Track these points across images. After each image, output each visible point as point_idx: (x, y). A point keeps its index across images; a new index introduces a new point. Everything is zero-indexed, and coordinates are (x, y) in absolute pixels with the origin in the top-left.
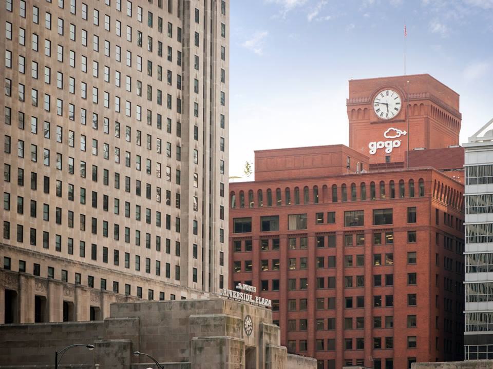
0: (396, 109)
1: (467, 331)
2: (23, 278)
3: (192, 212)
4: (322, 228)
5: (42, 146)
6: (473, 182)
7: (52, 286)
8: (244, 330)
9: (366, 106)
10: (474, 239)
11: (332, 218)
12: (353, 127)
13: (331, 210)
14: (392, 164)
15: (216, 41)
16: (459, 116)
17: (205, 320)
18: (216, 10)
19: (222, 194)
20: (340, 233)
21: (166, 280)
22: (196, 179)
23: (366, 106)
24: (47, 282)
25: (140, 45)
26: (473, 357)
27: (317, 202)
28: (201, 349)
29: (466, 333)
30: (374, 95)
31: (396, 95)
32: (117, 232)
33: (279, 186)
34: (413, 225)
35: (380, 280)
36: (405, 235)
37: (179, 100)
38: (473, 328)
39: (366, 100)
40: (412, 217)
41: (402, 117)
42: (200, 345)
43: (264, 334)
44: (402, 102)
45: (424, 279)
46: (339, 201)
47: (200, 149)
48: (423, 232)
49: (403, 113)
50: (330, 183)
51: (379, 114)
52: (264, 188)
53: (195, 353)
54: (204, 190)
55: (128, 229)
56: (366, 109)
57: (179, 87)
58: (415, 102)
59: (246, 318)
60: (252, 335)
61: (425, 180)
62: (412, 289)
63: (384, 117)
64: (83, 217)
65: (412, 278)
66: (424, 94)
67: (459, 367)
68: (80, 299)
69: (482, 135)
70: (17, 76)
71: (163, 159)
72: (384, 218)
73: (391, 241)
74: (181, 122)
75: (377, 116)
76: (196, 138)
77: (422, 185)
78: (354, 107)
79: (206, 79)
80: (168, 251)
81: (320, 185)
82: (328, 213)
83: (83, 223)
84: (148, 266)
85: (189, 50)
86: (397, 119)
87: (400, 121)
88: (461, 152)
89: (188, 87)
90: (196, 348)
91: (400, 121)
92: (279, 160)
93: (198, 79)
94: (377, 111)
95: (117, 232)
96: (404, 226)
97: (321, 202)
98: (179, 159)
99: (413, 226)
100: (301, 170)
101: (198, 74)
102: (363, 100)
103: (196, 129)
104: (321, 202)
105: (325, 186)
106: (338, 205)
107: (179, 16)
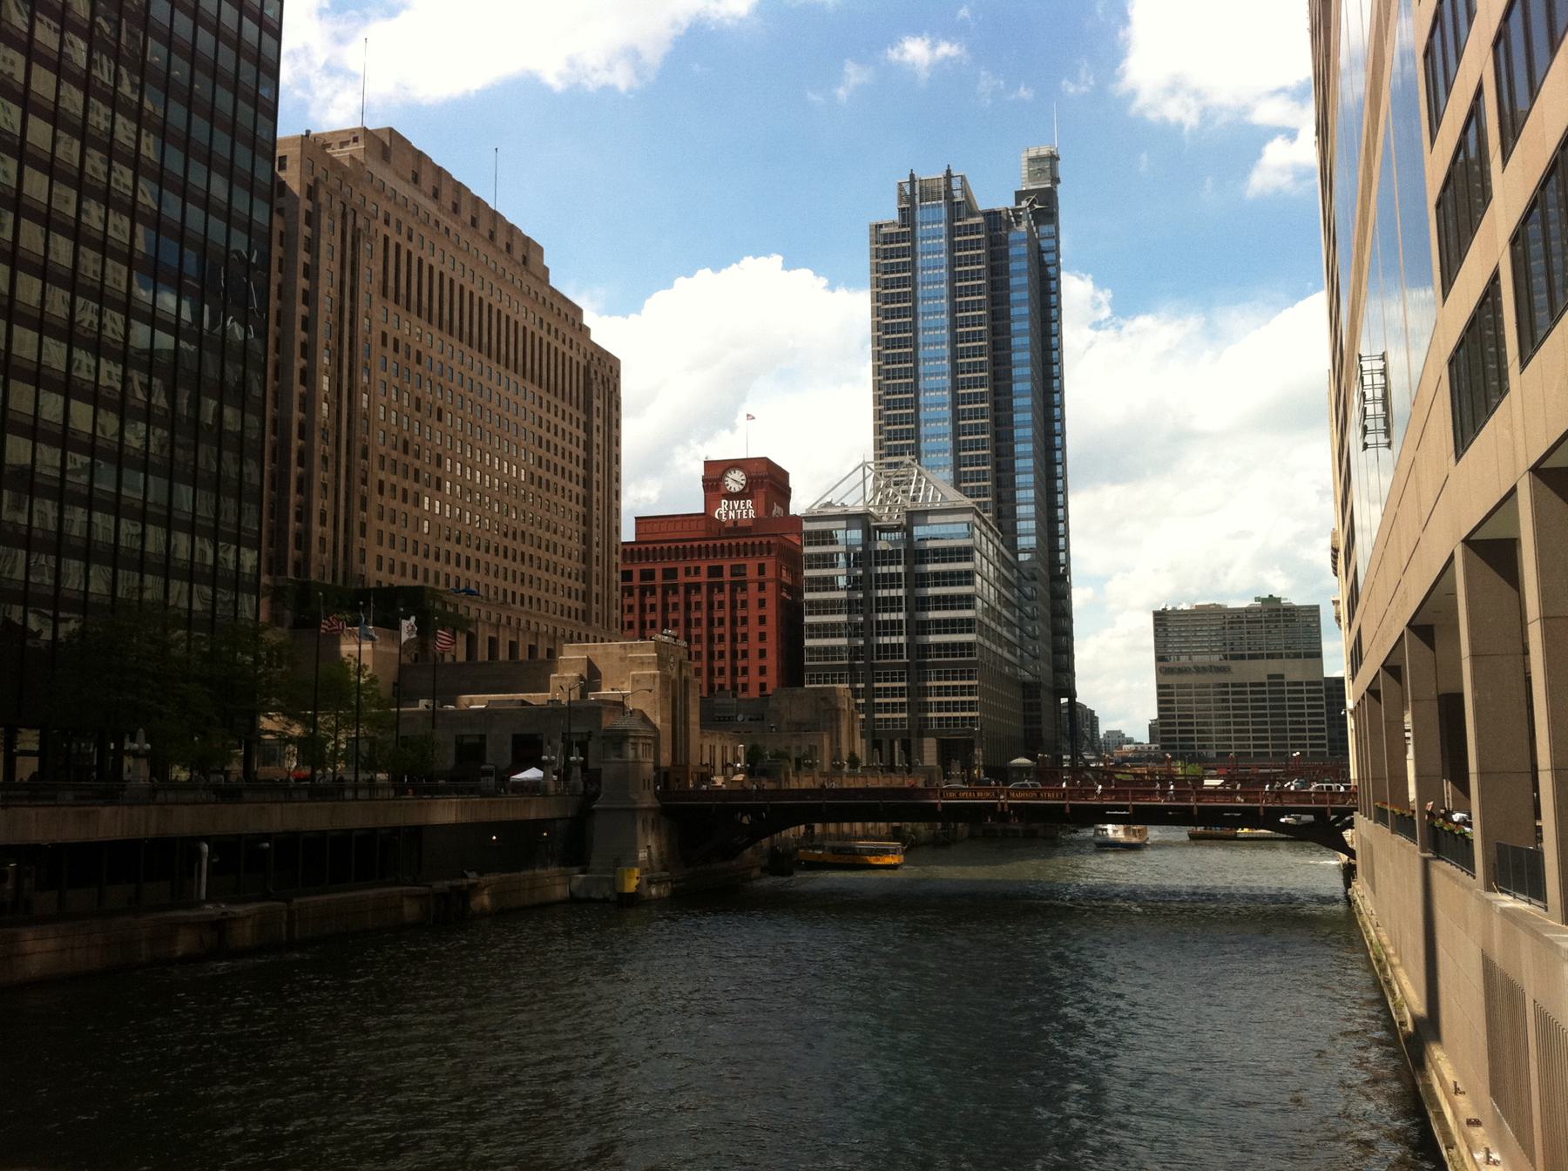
2: (480, 624)
3: (595, 529)
4: (690, 579)
6: (810, 544)
7: (501, 629)
11: (697, 570)
12: (1044, 648)
16: (790, 490)
17: (641, 658)
19: (617, 553)
21: (575, 621)
24: (497, 626)
31: (741, 473)
32: (478, 566)
33: (663, 545)
34: (762, 577)
36: (756, 585)
38: (811, 660)
45: (772, 620)
47: (601, 517)
52: (643, 547)
55: (449, 552)
57: (584, 468)
62: (762, 629)
64: (514, 572)
65: (762, 620)
68: (521, 639)
69: (816, 507)
71: (573, 525)
80: (577, 599)
83: (514, 577)
84: (562, 611)
88: (798, 520)
95: (478, 566)
98: (584, 525)
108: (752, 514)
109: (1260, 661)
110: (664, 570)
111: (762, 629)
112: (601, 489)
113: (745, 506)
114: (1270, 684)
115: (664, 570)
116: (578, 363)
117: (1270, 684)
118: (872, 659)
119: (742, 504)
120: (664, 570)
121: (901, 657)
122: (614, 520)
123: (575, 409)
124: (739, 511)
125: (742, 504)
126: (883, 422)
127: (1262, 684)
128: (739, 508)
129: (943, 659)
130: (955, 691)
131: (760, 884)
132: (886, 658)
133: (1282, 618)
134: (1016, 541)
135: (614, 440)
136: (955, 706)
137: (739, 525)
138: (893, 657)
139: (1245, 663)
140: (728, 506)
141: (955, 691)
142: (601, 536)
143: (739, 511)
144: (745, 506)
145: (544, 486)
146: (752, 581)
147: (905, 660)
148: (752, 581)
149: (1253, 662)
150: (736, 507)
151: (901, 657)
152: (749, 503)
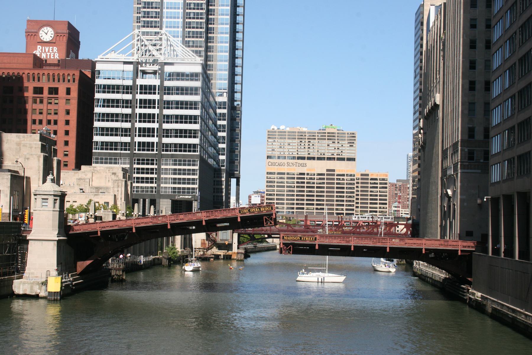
1: (94, 150)
9: (36, 34)
10: (99, 106)
14: (48, 64)
16: (79, 42)
20: (30, 97)
23: (36, 34)
26: (97, 163)
27: (54, 82)
28: (28, 159)
34: (68, 96)
35: (489, 155)
39: (35, 31)
41: (54, 41)
42: (28, 157)
46: (31, 81)
48: (73, 100)
49: (54, 39)
50: (26, 72)
51: (42, 38)
53: (25, 160)
56: (35, 35)
58: (61, 34)
61: (76, 75)
63: (45, 40)
65: (67, 122)
72: (54, 91)
73: (57, 104)
75: (41, 39)
77: (74, 77)
78: (29, 34)
87: (53, 43)
90: (25, 158)
91: (53, 43)
100: (11, 64)
106: (30, 83)
108: (57, 56)
109: (344, 162)
110: (50, 88)
111: (67, 128)
113: (53, 50)
114: (328, 175)
115: (50, 88)
117: (328, 175)
118: (135, 150)
119: (51, 49)
120: (50, 88)
121: (153, 150)
124: (48, 54)
125: (51, 49)
126: (141, 6)
127: (323, 175)
128: (49, 51)
129: (178, 153)
130: (184, 172)
131: (465, 244)
132: (144, 150)
133: (336, 135)
136: (184, 181)
137: (48, 62)
138: (148, 150)
139: (316, 162)
140: (42, 50)
141: (184, 172)
143: (48, 54)
144: (53, 50)
147: (155, 152)
149: (328, 161)
150: (47, 51)
151: (153, 150)
152: (55, 49)
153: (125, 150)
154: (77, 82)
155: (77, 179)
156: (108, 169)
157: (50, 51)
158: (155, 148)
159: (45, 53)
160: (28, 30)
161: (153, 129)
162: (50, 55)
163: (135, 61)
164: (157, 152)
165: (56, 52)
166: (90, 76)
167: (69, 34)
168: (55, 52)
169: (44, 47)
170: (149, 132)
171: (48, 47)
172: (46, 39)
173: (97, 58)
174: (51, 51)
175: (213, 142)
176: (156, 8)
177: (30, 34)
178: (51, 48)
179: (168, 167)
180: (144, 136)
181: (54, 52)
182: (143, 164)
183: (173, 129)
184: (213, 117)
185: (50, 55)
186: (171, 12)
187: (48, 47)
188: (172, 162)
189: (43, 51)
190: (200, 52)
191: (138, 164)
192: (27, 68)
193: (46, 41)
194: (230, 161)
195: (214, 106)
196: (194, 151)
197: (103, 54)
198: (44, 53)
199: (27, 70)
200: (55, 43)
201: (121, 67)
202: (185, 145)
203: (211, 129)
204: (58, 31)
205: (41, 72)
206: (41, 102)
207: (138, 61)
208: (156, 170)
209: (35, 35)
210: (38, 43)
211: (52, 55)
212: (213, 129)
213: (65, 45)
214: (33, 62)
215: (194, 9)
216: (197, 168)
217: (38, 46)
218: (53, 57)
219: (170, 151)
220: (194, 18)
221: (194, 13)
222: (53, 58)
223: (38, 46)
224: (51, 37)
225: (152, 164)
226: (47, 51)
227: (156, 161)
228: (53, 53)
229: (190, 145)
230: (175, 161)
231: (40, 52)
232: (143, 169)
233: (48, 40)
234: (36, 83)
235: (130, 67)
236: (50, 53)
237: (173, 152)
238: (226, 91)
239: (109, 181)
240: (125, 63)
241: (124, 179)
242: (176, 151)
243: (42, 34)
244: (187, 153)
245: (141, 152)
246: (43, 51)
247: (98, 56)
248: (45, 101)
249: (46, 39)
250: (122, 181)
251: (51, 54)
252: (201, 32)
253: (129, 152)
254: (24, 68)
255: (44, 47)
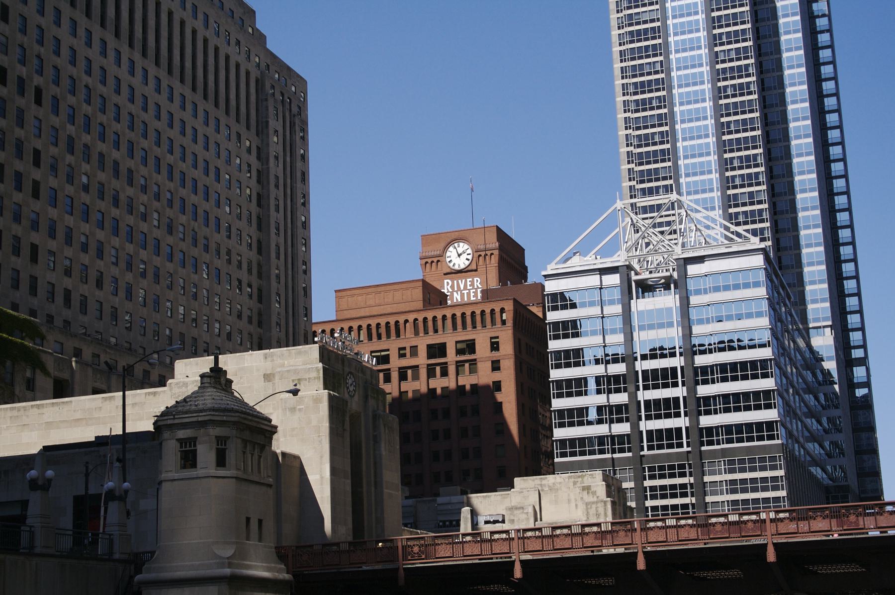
0: (467, 259)
1: (557, 457)
3: (274, 283)
5: (110, 244)
8: (346, 389)
11: (414, 350)
13: (414, 344)
15: (297, 232)
16: (526, 268)
18: (295, 135)
22: (278, 294)
25: (229, 237)
29: (556, 460)
30: (446, 248)
36: (489, 364)
37: (259, 218)
38: (563, 455)
39: (438, 252)
40: (495, 346)
41: (474, 267)
43: (370, 397)
44: (473, 252)
48: (507, 360)
49: (474, 262)
50: (411, 317)
51: (451, 265)
54: (287, 312)
56: (438, 261)
59: (348, 375)
60: (356, 398)
63: (456, 267)
66: (494, 244)
67: (567, 480)
70: (81, 165)
72: (470, 347)
74: (261, 240)
75: (449, 267)
76: (278, 258)
78: (426, 260)
79: (287, 200)
81: (401, 319)
82: (411, 347)
85: (268, 168)
86: (469, 268)
89: (269, 205)
92: (360, 298)
93: (279, 293)
94: (449, 262)
96: (488, 355)
97: (403, 337)
99: (496, 355)
100: (382, 307)
101: (279, 287)
102: (435, 253)
103: (277, 246)
104: (403, 337)
105: (444, 317)
106: (420, 338)
107: (257, 135)
112: (282, 257)
113: (472, 284)
116: (248, 73)
119: (469, 283)
121: (680, 445)
122: (299, 184)
123: (244, 129)
124: (465, 292)
128: (465, 288)
132: (660, 447)
134: (817, 39)
135: (299, 175)
138: (670, 446)
140: (452, 287)
142: (282, 268)
144: (472, 284)
145: (201, 219)
146: (484, 360)
147: (685, 449)
148: (484, 360)
150: (462, 287)
151: (680, 445)
153: (622, 451)
154: (510, 323)
155: (506, 509)
156: (573, 480)
157: (469, 288)
158: (685, 441)
159: (459, 293)
160: (424, 254)
161: (676, 399)
162: (469, 294)
163: (623, 264)
164: (689, 449)
165: (480, 286)
166: (542, 317)
167: (501, 248)
168: (478, 288)
169: (455, 282)
170: (668, 408)
171: (464, 281)
172: (459, 265)
173: (546, 269)
174: (470, 286)
175: (816, 431)
176: (665, 178)
177: (429, 261)
178: (468, 280)
179: (717, 478)
180: (658, 417)
181: (476, 287)
182: (662, 476)
183: (719, 396)
184: (810, 380)
185: (469, 294)
186: (695, 182)
187: (464, 281)
188: (725, 465)
189: (456, 289)
190: (762, 230)
191: (652, 477)
192: (412, 309)
193: (459, 269)
194: (855, 451)
195: (810, 380)
196: (771, 437)
197: (556, 261)
198: (457, 292)
199: (411, 314)
200: (476, 270)
201: (593, 280)
202: (749, 426)
203: (812, 453)
204: (479, 247)
205: (439, 314)
206: (444, 373)
207: (628, 263)
208: (692, 487)
209: (438, 261)
210: (445, 274)
211: (472, 294)
212: (816, 452)
213: (494, 271)
214: (422, 296)
215: (741, 168)
216: (781, 473)
217: (446, 281)
218: (474, 297)
219: (718, 444)
220: (742, 186)
221: (742, 176)
222: (475, 299)
223: (446, 281)
224: (450, 261)
225: (683, 475)
226: (462, 288)
227: (690, 468)
228: (474, 290)
229: (759, 425)
230: (732, 462)
231: (450, 290)
232: (663, 488)
233: (462, 266)
234: (431, 337)
235: (614, 279)
236: (468, 291)
237: (723, 443)
238: (830, 323)
239: (576, 505)
240: (603, 271)
241: (609, 499)
242: (730, 441)
243: (450, 257)
244: (756, 443)
245: (656, 452)
246: (456, 289)
247: (548, 266)
248: (452, 369)
249: (459, 265)
250: (605, 502)
251: (470, 292)
252: (760, 211)
253: (630, 454)
254: (407, 310)
255: (455, 282)
